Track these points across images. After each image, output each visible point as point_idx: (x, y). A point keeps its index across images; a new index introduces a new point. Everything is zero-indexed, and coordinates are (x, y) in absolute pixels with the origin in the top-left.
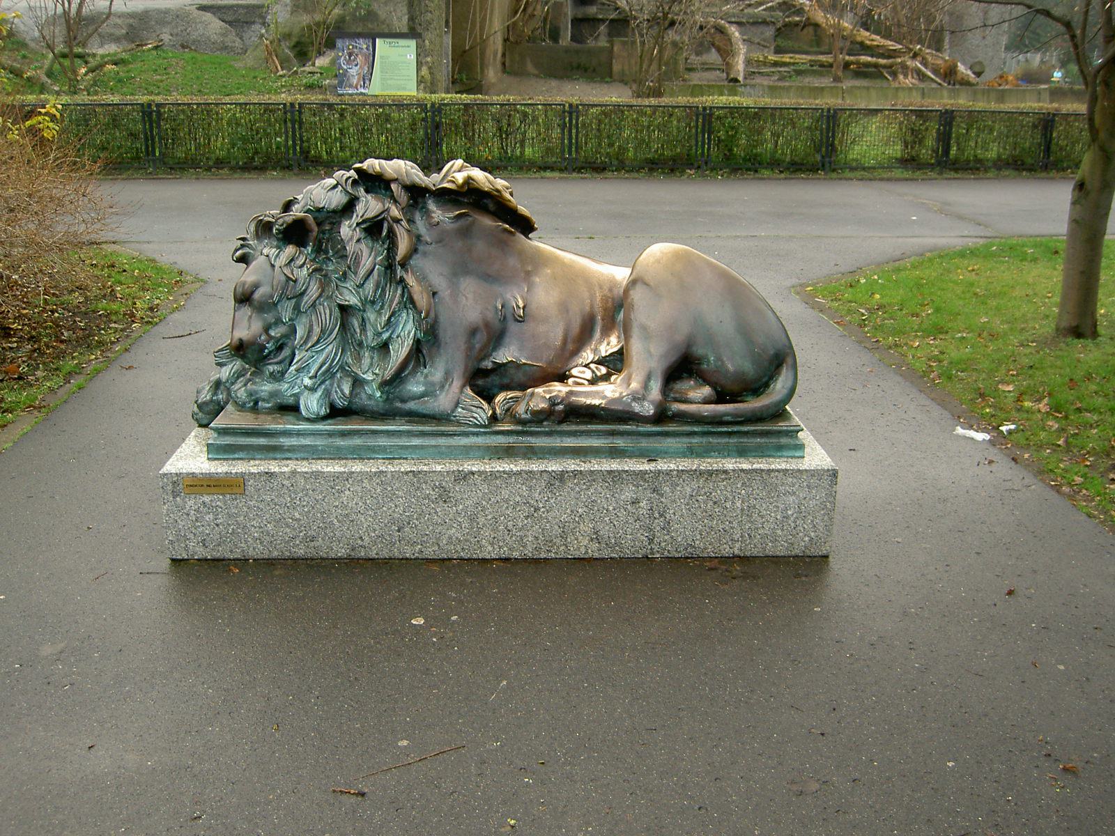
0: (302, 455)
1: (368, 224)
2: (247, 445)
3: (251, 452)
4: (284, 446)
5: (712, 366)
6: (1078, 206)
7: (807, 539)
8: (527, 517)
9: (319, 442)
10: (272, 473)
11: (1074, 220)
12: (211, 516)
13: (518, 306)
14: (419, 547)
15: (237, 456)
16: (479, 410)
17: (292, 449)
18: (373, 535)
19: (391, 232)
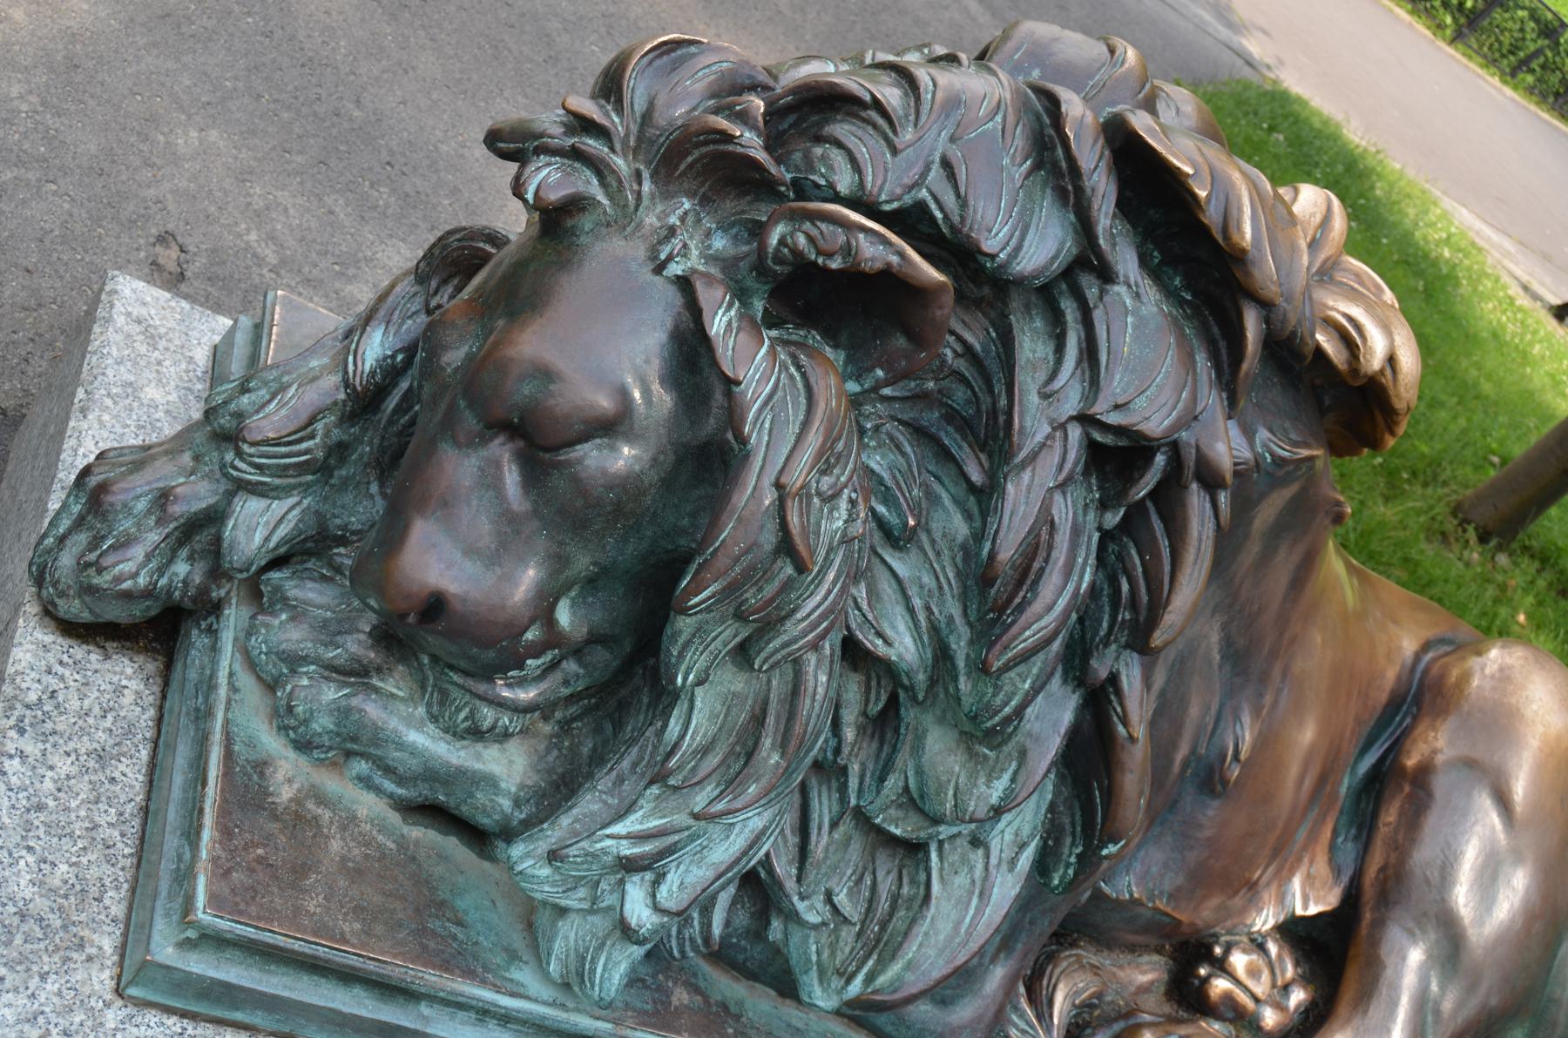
1: (1123, 443)
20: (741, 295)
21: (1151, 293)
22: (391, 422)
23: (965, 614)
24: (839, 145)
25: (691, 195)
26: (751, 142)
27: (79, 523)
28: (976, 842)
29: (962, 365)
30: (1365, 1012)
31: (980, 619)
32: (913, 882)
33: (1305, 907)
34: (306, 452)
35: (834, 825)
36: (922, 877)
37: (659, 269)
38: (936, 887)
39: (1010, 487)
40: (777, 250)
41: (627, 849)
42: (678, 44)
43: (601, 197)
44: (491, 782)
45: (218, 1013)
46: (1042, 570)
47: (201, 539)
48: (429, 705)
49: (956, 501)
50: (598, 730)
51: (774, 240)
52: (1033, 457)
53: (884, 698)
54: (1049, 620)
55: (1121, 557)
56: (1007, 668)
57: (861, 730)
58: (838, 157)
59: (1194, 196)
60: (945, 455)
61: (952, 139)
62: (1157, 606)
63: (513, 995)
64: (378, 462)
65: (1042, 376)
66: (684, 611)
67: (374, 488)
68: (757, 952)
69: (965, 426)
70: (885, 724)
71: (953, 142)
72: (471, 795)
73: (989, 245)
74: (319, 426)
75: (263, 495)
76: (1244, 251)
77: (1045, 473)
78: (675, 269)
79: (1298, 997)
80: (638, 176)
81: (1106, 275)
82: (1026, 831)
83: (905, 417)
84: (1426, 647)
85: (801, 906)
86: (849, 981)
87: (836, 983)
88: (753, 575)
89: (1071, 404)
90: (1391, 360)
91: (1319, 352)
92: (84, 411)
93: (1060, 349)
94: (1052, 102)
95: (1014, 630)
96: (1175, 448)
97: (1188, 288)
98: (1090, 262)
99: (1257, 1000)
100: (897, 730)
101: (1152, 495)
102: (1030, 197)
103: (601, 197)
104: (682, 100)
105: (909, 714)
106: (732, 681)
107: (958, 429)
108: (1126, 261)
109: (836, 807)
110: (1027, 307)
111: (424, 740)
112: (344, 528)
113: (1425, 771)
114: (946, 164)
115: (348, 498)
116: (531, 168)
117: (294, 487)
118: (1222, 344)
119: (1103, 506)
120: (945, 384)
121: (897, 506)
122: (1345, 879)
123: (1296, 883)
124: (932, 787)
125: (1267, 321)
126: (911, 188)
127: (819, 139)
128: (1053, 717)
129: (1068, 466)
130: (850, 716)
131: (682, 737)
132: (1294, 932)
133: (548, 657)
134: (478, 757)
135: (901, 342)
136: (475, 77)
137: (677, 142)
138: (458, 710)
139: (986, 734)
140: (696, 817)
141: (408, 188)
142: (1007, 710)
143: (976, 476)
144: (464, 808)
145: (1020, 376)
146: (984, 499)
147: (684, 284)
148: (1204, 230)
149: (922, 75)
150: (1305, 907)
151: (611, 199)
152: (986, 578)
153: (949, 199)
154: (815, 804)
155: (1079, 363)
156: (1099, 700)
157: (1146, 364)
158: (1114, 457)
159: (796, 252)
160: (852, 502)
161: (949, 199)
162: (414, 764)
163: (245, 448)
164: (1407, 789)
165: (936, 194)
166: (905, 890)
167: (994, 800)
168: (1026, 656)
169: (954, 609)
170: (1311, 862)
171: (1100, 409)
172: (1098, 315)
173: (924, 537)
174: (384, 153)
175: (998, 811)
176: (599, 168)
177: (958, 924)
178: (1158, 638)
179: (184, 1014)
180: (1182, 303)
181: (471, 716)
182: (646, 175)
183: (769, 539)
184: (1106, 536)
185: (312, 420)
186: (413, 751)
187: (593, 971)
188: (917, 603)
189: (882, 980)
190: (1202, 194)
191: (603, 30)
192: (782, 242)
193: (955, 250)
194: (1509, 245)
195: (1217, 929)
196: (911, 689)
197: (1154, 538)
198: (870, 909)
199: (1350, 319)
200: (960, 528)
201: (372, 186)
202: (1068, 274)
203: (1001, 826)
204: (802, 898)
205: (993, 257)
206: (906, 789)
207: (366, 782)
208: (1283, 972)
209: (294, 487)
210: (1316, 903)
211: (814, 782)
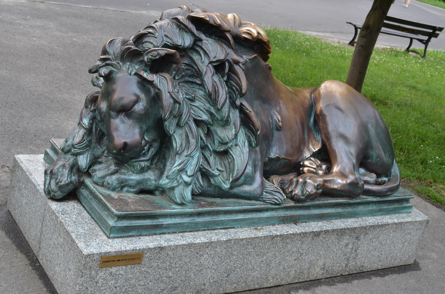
0: (173, 230)
1: (219, 63)
2: (139, 226)
3: (141, 231)
4: (163, 225)
5: (374, 161)
6: (364, 39)
7: (407, 256)
8: (295, 260)
9: (186, 220)
10: (163, 247)
11: (361, 46)
12: (113, 282)
13: (279, 120)
14: (235, 285)
15: (130, 234)
16: (277, 194)
17: (168, 226)
18: (212, 281)
19: (232, 70)
20: (146, 71)
21: (210, 40)
22: (96, 133)
23: (211, 105)
24: (147, 42)
25: (128, 62)
26: (133, 47)
27: (51, 178)
28: (236, 145)
29: (186, 67)
30: (337, 160)
31: (213, 103)
32: (230, 158)
33: (315, 150)
34: (85, 143)
35: (211, 155)
36: (231, 156)
37: (130, 74)
38: (234, 156)
39: (205, 79)
40: (147, 61)
41: (178, 168)
42: (112, 41)
43: (114, 69)
44: (149, 179)
45: (127, 235)
46: (218, 89)
47: (75, 170)
48: (131, 171)
49: (199, 89)
50: (162, 162)
51: (146, 59)
52: (206, 73)
53: (206, 129)
54: (224, 96)
55: (231, 84)
56: (222, 108)
57: (206, 137)
58: (148, 44)
59: (207, 20)
60: (193, 83)
61: (164, 31)
62: (241, 87)
63: (174, 209)
64: (97, 141)
65: (200, 61)
66: (165, 120)
67: (99, 147)
68: (211, 190)
69: (192, 76)
70: (209, 134)
71: (165, 35)
72: (147, 184)
73: (179, 44)
74: (85, 138)
75: (82, 154)
76: (220, 24)
77: (209, 74)
78: (133, 73)
79: (324, 167)
80: (118, 63)
81: (201, 40)
82: (244, 139)
83: (182, 81)
84: (311, 94)
85: (214, 172)
86: (229, 180)
87: (227, 182)
88: (173, 109)
89: (207, 62)
90: (258, 33)
91: (244, 37)
92: (31, 175)
93: (200, 55)
94: (176, 19)
95: (219, 100)
96: (227, 60)
97: (216, 37)
98: (197, 40)
99: (315, 169)
100: (212, 134)
101: (229, 70)
102: (181, 34)
103: (114, 69)
104: (117, 48)
105: (212, 128)
106: (179, 131)
107: (192, 77)
108: (203, 36)
109: (209, 153)
110: (192, 53)
111: (135, 177)
112: (98, 155)
113: (321, 111)
114: (165, 36)
115: (96, 150)
116: (100, 71)
117: (86, 151)
118: (227, 42)
119: (223, 77)
120: (186, 72)
121: (189, 94)
122: (320, 142)
123: (311, 146)
124: (223, 139)
125: (231, 34)
126: (162, 42)
127: (143, 43)
128: (235, 116)
129: (212, 71)
130: (202, 135)
131: (176, 145)
132: (314, 155)
133: (147, 146)
134: (144, 176)
135: (174, 66)
136: (39, 112)
137: (122, 53)
138: (137, 166)
139: (226, 123)
140: (186, 156)
141: (43, 138)
142: (226, 115)
143: (199, 82)
144: (147, 187)
145: (196, 62)
146: (202, 85)
147: (136, 74)
148: (212, 25)
149: (154, 25)
150: (315, 150)
151: (116, 69)
152: (210, 95)
153: (169, 40)
154: (206, 154)
155: (204, 55)
156: (241, 109)
157: (214, 50)
158: (219, 67)
159: (151, 59)
160: (181, 92)
161: (169, 40)
162: (134, 182)
163: (75, 146)
164: (321, 117)
165: (167, 41)
166: (230, 160)
167: (234, 134)
168: (224, 104)
169: (208, 105)
170: (312, 142)
171: (212, 59)
172: (203, 47)
173: (197, 98)
174: (32, 134)
175: (236, 135)
176: (111, 65)
177: (241, 159)
178: (244, 91)
179: (121, 237)
180: (216, 40)
181: (140, 166)
182: (119, 62)
183: (172, 101)
184: (226, 82)
185: (83, 137)
186: (133, 180)
187: (185, 195)
188: (202, 109)
189: (234, 175)
190: (208, 19)
191: (58, 90)
192: (147, 59)
193: (176, 47)
194: (330, 35)
195: (299, 160)
196: (210, 123)
197: (234, 78)
198: (225, 166)
199: (247, 30)
200: (202, 93)
201: (35, 141)
202: (195, 43)
203: (239, 140)
204: (213, 171)
205: (181, 45)
206: (219, 142)
207: (128, 192)
208: (318, 163)
209: (86, 151)
210: (317, 148)
211: (203, 152)
